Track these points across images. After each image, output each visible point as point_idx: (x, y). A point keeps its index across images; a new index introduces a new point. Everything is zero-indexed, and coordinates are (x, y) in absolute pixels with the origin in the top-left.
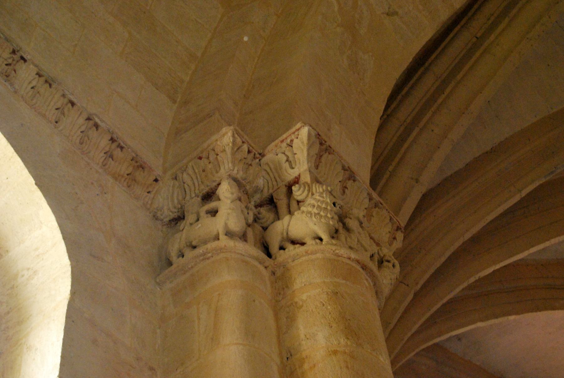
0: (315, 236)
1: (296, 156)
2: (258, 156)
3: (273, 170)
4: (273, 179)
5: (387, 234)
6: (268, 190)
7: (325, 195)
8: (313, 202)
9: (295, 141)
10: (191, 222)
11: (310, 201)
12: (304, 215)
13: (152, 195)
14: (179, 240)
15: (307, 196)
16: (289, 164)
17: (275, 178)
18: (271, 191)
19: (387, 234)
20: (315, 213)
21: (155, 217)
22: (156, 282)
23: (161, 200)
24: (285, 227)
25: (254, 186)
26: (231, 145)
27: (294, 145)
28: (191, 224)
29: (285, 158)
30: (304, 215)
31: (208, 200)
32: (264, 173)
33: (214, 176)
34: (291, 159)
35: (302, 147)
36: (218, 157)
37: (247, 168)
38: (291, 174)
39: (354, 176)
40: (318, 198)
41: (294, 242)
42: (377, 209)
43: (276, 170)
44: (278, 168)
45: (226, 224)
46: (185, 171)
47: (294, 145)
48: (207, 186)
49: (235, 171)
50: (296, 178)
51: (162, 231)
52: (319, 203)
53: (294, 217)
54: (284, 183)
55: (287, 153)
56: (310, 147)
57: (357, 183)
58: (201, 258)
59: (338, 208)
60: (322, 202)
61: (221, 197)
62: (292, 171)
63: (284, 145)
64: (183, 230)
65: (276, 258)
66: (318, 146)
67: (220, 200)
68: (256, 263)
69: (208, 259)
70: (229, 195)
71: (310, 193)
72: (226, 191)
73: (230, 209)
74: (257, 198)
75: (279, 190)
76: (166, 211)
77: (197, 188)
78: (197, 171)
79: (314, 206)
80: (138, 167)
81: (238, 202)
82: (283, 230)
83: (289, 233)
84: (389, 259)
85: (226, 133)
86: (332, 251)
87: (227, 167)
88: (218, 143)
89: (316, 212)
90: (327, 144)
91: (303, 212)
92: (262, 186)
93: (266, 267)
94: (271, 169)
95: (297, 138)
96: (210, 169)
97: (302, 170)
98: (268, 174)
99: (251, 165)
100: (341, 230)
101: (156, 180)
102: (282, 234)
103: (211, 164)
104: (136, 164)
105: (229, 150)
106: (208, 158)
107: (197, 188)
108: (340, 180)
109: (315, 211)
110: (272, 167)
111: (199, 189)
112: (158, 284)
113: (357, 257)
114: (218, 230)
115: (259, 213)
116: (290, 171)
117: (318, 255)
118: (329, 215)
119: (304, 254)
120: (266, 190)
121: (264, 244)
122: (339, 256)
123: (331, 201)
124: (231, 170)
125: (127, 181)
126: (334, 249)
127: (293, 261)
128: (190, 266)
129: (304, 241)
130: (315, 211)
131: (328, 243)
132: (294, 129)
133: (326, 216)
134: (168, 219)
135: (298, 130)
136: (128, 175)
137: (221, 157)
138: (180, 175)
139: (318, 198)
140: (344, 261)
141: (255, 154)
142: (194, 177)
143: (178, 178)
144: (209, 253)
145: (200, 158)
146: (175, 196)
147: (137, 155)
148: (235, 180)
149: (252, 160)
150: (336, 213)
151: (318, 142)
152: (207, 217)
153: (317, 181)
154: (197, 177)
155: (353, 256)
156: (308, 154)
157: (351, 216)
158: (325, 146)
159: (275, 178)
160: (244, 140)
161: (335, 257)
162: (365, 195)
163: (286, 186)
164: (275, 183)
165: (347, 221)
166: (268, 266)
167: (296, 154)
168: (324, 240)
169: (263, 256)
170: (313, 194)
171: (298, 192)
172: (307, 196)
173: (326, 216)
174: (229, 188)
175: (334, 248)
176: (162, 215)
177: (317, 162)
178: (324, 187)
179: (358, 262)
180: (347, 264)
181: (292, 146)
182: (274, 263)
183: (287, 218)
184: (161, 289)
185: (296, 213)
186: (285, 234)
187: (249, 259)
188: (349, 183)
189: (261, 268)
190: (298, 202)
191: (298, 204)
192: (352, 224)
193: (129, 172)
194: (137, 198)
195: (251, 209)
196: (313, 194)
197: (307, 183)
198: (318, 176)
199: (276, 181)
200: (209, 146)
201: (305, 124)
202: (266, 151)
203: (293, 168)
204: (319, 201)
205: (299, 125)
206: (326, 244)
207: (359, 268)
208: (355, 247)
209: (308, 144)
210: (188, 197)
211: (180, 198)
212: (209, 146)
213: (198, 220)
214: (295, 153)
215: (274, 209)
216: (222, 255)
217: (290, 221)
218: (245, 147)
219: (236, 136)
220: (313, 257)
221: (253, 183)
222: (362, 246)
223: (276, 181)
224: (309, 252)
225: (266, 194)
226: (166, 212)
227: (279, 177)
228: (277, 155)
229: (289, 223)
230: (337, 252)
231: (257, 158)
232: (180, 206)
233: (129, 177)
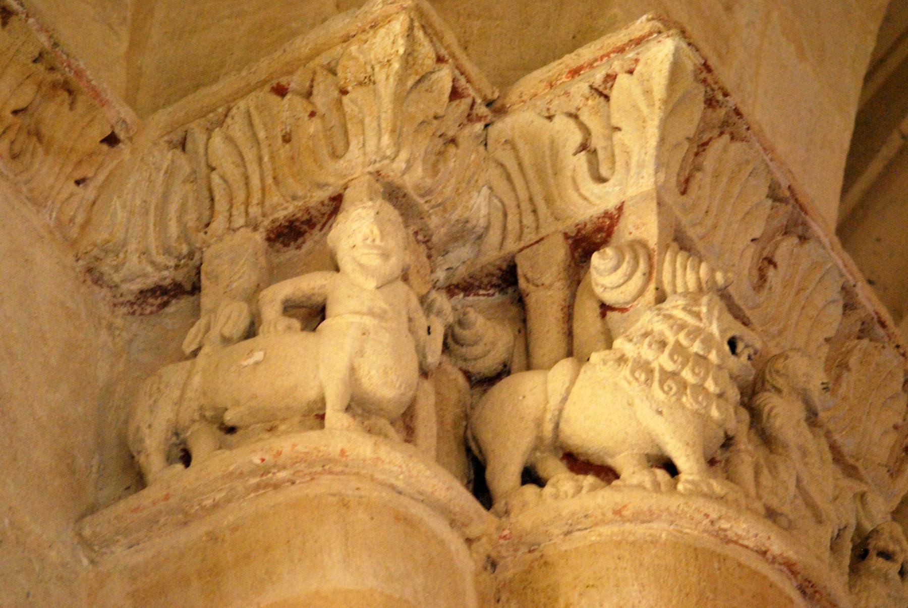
0: (655, 451)
1: (617, 136)
2: (482, 110)
3: (531, 174)
4: (526, 205)
5: (885, 433)
6: (504, 238)
7: (704, 309)
8: (660, 327)
9: (623, 79)
10: (227, 333)
11: (648, 319)
12: (626, 371)
13: (89, 193)
14: (176, 394)
15: (641, 292)
16: (590, 162)
17: (531, 200)
18: (511, 246)
19: (885, 433)
20: (662, 370)
21: (93, 275)
22: (80, 535)
23: (121, 215)
24: (554, 402)
25: (454, 217)
26: (396, 66)
27: (614, 95)
28: (226, 341)
29: (577, 138)
30: (626, 371)
31: (286, 245)
32: (493, 174)
33: (321, 167)
34: (597, 142)
35: (645, 110)
36: (346, 99)
37: (440, 153)
38: (588, 201)
39: (804, 224)
40: (679, 314)
41: (578, 463)
42: (865, 342)
43: (540, 171)
44: (548, 166)
45: (353, 370)
46: (221, 123)
47: (615, 94)
48: (294, 198)
49: (400, 164)
50: (606, 214)
51: (110, 327)
52: (682, 337)
53: (586, 372)
54: (561, 227)
55: (585, 117)
56: (673, 108)
57: (809, 246)
58: (254, 481)
59: (744, 358)
60: (694, 333)
61: (344, 260)
62: (598, 188)
63: (580, 87)
64: (195, 354)
65: (507, 513)
66: (698, 108)
67: (337, 269)
68: (439, 526)
69: (277, 486)
70: (373, 260)
71: (652, 286)
72: (362, 236)
73: (371, 313)
74: (461, 259)
75: (541, 248)
76: (134, 258)
77: (256, 198)
78: (262, 135)
79: (663, 344)
80: (54, 86)
81: (401, 286)
82: (545, 410)
83: (562, 425)
84: (891, 547)
85: (387, 19)
86: (706, 522)
87: (371, 145)
88: (354, 49)
89: (670, 367)
90: (732, 101)
91: (622, 360)
92: (482, 222)
93: (469, 541)
94: (520, 165)
95: (631, 72)
96: (312, 137)
97: (632, 191)
98: (509, 179)
99: (453, 141)
100: (746, 444)
101: (111, 140)
102: (539, 423)
103: (316, 120)
104: (51, 77)
105: (386, 85)
106: (309, 94)
107: (256, 198)
108: (757, 234)
109: (664, 361)
110: (527, 161)
111: (262, 203)
112: (86, 544)
113: (791, 554)
114: (321, 388)
115: (460, 323)
116: (590, 188)
117: (655, 525)
118: (710, 385)
119: (610, 515)
120: (494, 236)
121: (468, 450)
122: (729, 541)
123: (722, 332)
124: (385, 157)
125: (11, 135)
126: (714, 516)
127: (568, 533)
128: (208, 502)
129: (610, 462)
130: (664, 361)
131: (695, 492)
132: (620, 37)
133: (700, 388)
134: (136, 286)
135: (638, 42)
136: (15, 112)
137: (353, 101)
138: (198, 137)
139: (679, 314)
140: (743, 559)
141: (473, 103)
142: (250, 155)
143: (189, 146)
144: (284, 468)
145: (281, 91)
146: (173, 208)
147: (56, 45)
148: (394, 195)
149: (461, 126)
150: (733, 378)
151: (701, 98)
152: (289, 328)
153: (679, 240)
154: (260, 159)
155: (777, 547)
156: (662, 140)
157: (780, 382)
158: (722, 113)
159: (531, 200)
160: (443, 52)
162: (833, 292)
163: (566, 236)
164: (528, 220)
165: (770, 402)
166: (478, 539)
167: (619, 129)
168: (683, 477)
169: (462, 498)
170: (661, 298)
171: (607, 274)
172: (641, 292)
173: (700, 388)
174: (376, 232)
175: (714, 510)
176: (116, 269)
177: (686, 167)
178: (704, 269)
179: (790, 568)
180: (754, 573)
181: (607, 98)
182: (500, 528)
183: (563, 369)
184: (92, 562)
185: (595, 357)
186: (548, 427)
187: (418, 511)
188: (786, 248)
189: (455, 543)
190: (605, 308)
191: (603, 315)
192: (784, 414)
193: (21, 104)
194: (37, 202)
195: (439, 313)
196: (661, 298)
197: (644, 244)
198: (685, 221)
199: (535, 211)
200: (316, 53)
201: (668, 23)
202: (513, 97)
203: (601, 180)
204: (682, 327)
205: (642, 25)
206: (690, 494)
207: (789, 588)
208: (786, 509)
209: (665, 102)
210: (219, 224)
211: (191, 219)
212: (316, 53)
213: (251, 332)
214: (612, 130)
215: (514, 310)
216: (325, 485)
217: (573, 382)
218: (444, 77)
219: (419, 34)
220: (640, 530)
221: (454, 207)
222: (810, 504)
223: (535, 211)
224: (627, 513)
225: (492, 253)
226: (134, 262)
227: (548, 200)
228: (550, 118)
229: (568, 391)
230: (724, 525)
231: (479, 119)
232: (185, 249)
233: (18, 120)
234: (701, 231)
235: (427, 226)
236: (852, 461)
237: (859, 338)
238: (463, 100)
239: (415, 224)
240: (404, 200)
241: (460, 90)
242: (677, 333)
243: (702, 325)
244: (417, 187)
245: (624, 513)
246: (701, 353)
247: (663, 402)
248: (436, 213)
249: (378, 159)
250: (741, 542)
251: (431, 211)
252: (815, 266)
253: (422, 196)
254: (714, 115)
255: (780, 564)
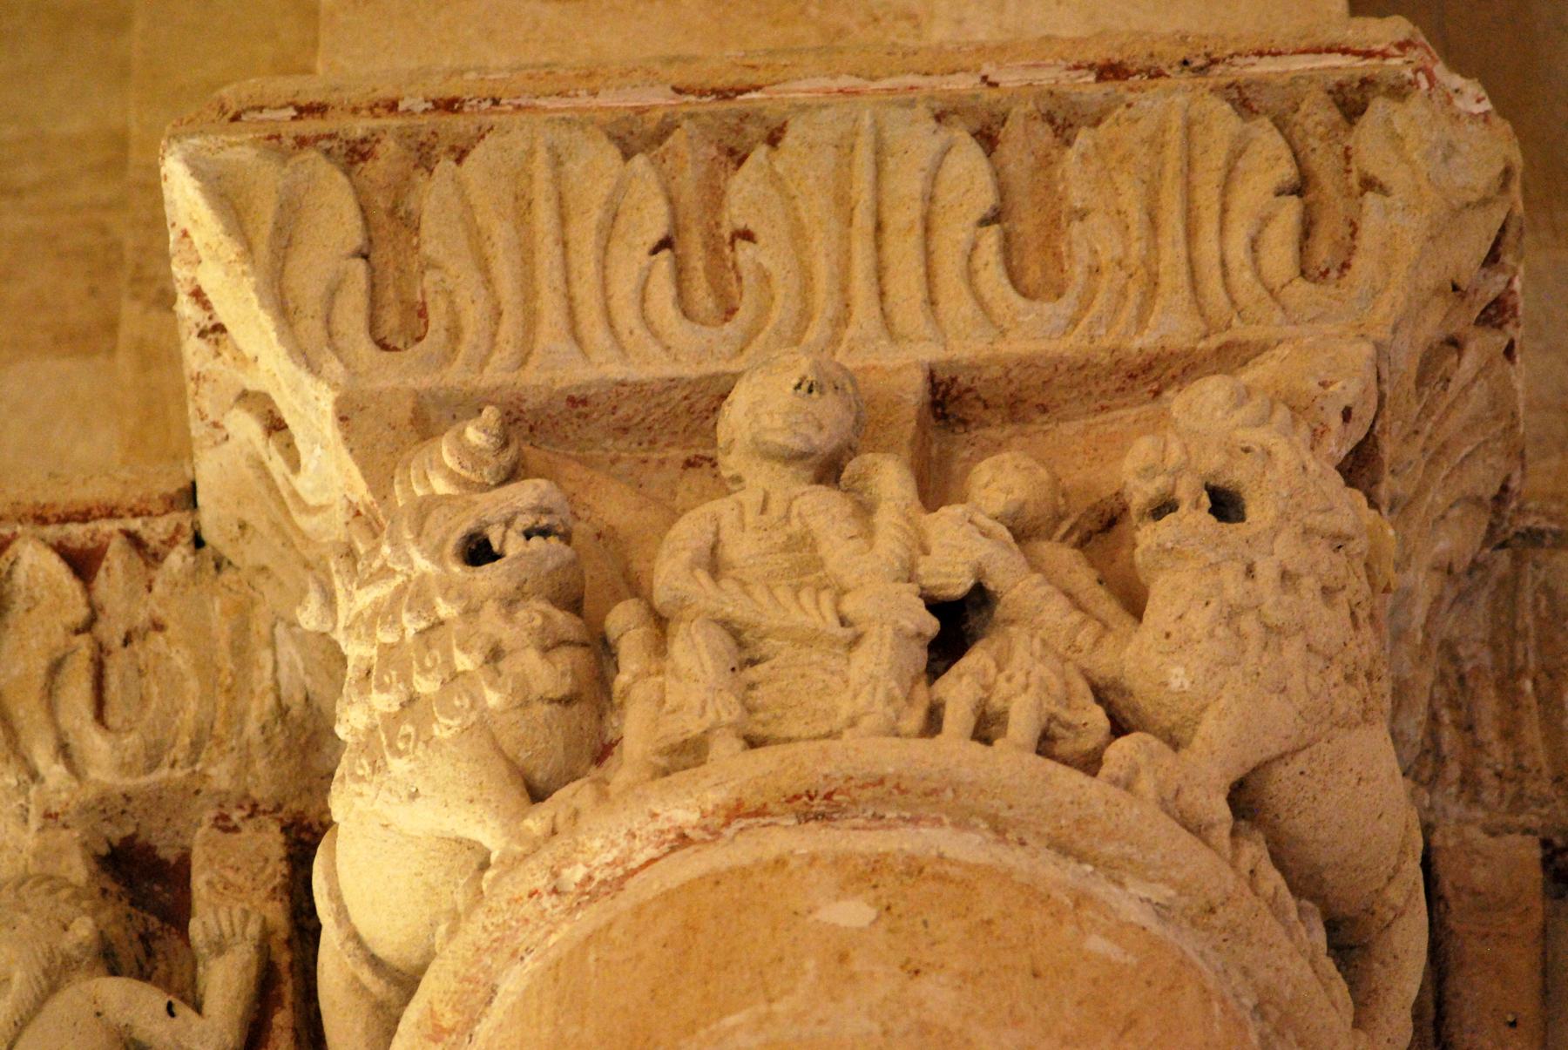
83: (382, 951)
86: (547, 902)
113: (713, 797)
122: (620, 883)
126: (542, 882)
161: (588, 919)
234: (503, 356)
235: (218, 792)
236: (1215, 342)
237: (1068, 143)
238: (109, 554)
239: (202, 808)
240: (136, 803)
241: (90, 545)
242: (371, 635)
243: (399, 579)
244: (124, 767)
245: (447, 1023)
246: (423, 624)
247: (411, 771)
248: (211, 762)
249: (22, 801)
250: (633, 865)
251: (198, 767)
252: (845, 148)
253: (152, 766)
254: (381, 163)
255: (727, 824)
